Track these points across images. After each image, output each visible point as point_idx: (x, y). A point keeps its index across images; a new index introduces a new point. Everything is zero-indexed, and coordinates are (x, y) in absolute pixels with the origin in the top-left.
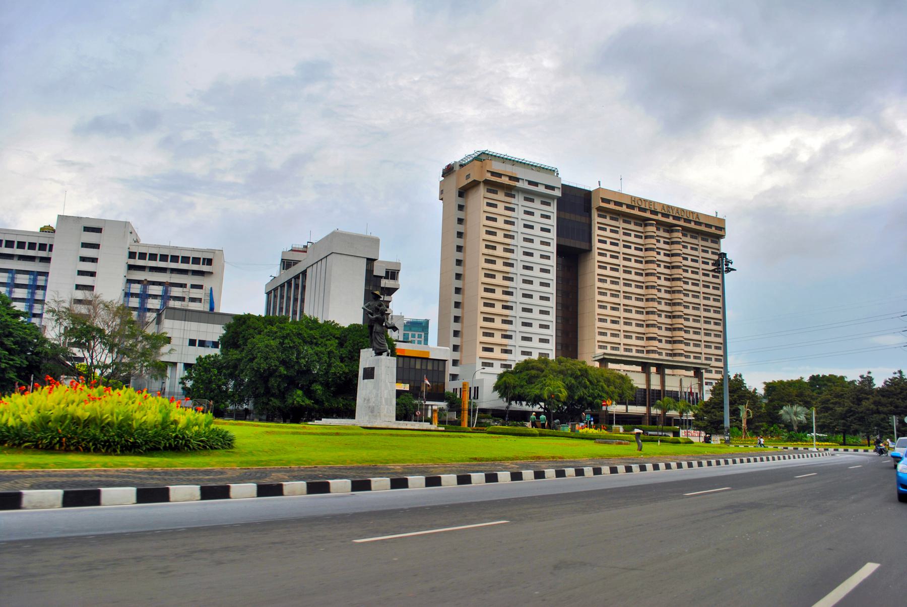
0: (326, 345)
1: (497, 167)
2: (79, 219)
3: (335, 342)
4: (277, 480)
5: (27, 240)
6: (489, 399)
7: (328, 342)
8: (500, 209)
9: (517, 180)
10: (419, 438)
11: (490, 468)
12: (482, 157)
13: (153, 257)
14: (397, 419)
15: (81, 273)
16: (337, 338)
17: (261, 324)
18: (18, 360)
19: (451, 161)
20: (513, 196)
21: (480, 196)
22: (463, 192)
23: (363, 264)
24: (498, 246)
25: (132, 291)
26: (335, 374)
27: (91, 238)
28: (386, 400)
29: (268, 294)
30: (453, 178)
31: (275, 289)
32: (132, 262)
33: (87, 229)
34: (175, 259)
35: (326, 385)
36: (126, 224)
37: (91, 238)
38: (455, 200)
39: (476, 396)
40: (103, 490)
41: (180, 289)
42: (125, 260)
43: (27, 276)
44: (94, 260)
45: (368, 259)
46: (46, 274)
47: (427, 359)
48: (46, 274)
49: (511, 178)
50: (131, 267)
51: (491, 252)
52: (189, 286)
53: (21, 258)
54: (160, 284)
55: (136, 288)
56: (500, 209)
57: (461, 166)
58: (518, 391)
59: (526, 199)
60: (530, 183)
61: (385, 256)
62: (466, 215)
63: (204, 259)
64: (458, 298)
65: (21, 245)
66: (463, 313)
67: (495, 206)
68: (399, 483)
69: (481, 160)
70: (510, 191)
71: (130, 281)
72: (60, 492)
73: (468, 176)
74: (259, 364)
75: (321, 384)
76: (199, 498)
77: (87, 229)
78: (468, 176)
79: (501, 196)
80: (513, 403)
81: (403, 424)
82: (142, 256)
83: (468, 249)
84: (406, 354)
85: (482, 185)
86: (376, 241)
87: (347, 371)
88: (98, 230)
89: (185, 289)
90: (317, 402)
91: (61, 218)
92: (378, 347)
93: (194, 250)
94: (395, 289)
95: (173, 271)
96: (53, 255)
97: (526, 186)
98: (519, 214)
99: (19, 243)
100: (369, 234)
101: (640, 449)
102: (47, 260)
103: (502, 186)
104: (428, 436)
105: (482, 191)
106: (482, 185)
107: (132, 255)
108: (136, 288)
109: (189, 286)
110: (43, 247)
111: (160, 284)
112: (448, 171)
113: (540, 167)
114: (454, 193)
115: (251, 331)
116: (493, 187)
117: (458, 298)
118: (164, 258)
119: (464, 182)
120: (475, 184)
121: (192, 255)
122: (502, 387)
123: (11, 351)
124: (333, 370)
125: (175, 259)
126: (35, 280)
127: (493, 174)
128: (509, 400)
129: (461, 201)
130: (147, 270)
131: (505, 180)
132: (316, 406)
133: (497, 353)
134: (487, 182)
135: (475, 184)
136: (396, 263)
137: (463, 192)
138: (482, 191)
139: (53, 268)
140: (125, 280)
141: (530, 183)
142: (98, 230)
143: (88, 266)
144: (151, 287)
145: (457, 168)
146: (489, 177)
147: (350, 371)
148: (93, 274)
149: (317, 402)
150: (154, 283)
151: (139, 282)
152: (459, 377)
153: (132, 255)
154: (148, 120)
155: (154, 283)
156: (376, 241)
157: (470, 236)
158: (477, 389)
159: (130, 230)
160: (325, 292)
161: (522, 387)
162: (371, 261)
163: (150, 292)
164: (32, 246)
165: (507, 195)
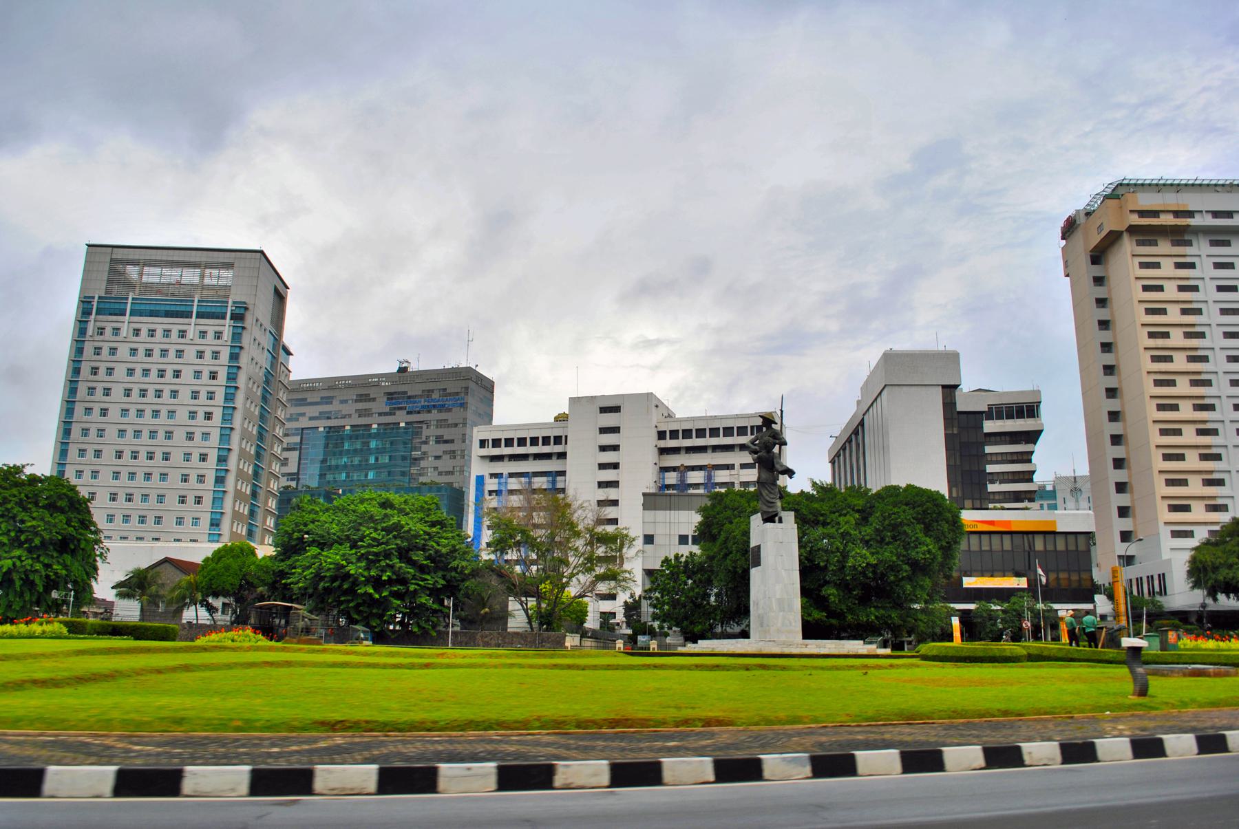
0: (838, 523)
1: (1147, 201)
2: (593, 398)
3: (853, 518)
4: (840, 745)
5: (540, 434)
6: (1183, 595)
7: (841, 519)
8: (1167, 268)
9: (1191, 214)
10: (841, 674)
11: (918, 736)
12: (1118, 192)
13: (687, 434)
14: (805, 637)
15: (602, 466)
16: (858, 511)
17: (743, 501)
18: (430, 580)
19: (1071, 212)
20: (1189, 243)
21: (1126, 258)
22: (1098, 256)
23: (937, 396)
24: (1172, 331)
25: (668, 482)
26: (854, 568)
27: (609, 420)
28: (780, 602)
29: (832, 462)
30: (1078, 237)
31: (838, 455)
32: (663, 444)
33: (604, 410)
34: (714, 432)
35: (844, 586)
36: (649, 396)
37: (609, 420)
38: (1087, 271)
39: (1163, 591)
40: (444, 767)
41: (726, 472)
42: (652, 442)
43: (544, 479)
44: (615, 448)
45: (944, 387)
46: (563, 473)
47: (1054, 533)
48: (563, 473)
49: (1177, 214)
50: (663, 451)
51: (1160, 342)
52: (737, 466)
53: (538, 456)
54: (700, 468)
55: (671, 478)
56: (1167, 268)
57: (1088, 214)
58: (1223, 575)
59: (1214, 243)
60: (1216, 214)
61: (979, 380)
62: (1109, 291)
63: (752, 427)
64: (1116, 428)
65: (534, 441)
66: (1128, 453)
67: (1157, 266)
68: (923, 760)
69: (1118, 197)
70: (1180, 235)
71: (664, 470)
72: (492, 766)
73: (1100, 227)
74: (735, 561)
75: (837, 586)
76: (494, 786)
77: (604, 410)
78: (1100, 227)
79: (1164, 247)
80: (1221, 597)
81: (815, 646)
82: (674, 435)
83: (1121, 347)
84: (1014, 529)
85: (1126, 237)
86: (952, 359)
87: (873, 561)
88: (616, 409)
89: (733, 472)
90: (832, 614)
91: (574, 401)
92: (765, 508)
93: (737, 417)
94: (1040, 432)
95: (715, 448)
96: (570, 449)
97: (1209, 221)
98: (1205, 271)
99: (532, 439)
100: (941, 348)
101: (1143, 691)
102: (562, 455)
103: (1163, 231)
104: (837, 668)
105: (1128, 245)
106: (1126, 237)
107: (661, 435)
108: (671, 478)
109: (737, 466)
110: (558, 440)
111: (700, 468)
112: (1070, 228)
113: (1231, 185)
114: (1083, 260)
115: (729, 513)
116: (1145, 234)
117: (1116, 428)
118: (701, 433)
119: (1096, 239)
120: (1113, 238)
121: (736, 424)
122: (1199, 572)
123: (422, 569)
124: (851, 562)
125: (714, 432)
126: (554, 482)
127: (1142, 213)
128: (1212, 593)
129: (1097, 271)
130: (683, 452)
131: (1167, 220)
132: (834, 621)
133: (1198, 512)
134: (1133, 230)
135: (1113, 238)
136: (1033, 392)
137: (1098, 256)
138: (1128, 245)
139: (570, 465)
140: (657, 467)
141: (1216, 214)
142: (616, 409)
143: (609, 457)
144: (691, 474)
145: (1082, 220)
146: (1135, 220)
147: (880, 561)
148: (615, 466)
149: (832, 614)
150: (693, 468)
151: (674, 469)
152: (1137, 560)
153: (661, 435)
154: (701, 269)
155: (693, 468)
156: (952, 359)
157: (1120, 324)
158: (1162, 577)
159: (655, 403)
160: (885, 449)
161: (1230, 566)
162: (950, 390)
163: (690, 481)
164: (546, 441)
165: (1176, 243)
